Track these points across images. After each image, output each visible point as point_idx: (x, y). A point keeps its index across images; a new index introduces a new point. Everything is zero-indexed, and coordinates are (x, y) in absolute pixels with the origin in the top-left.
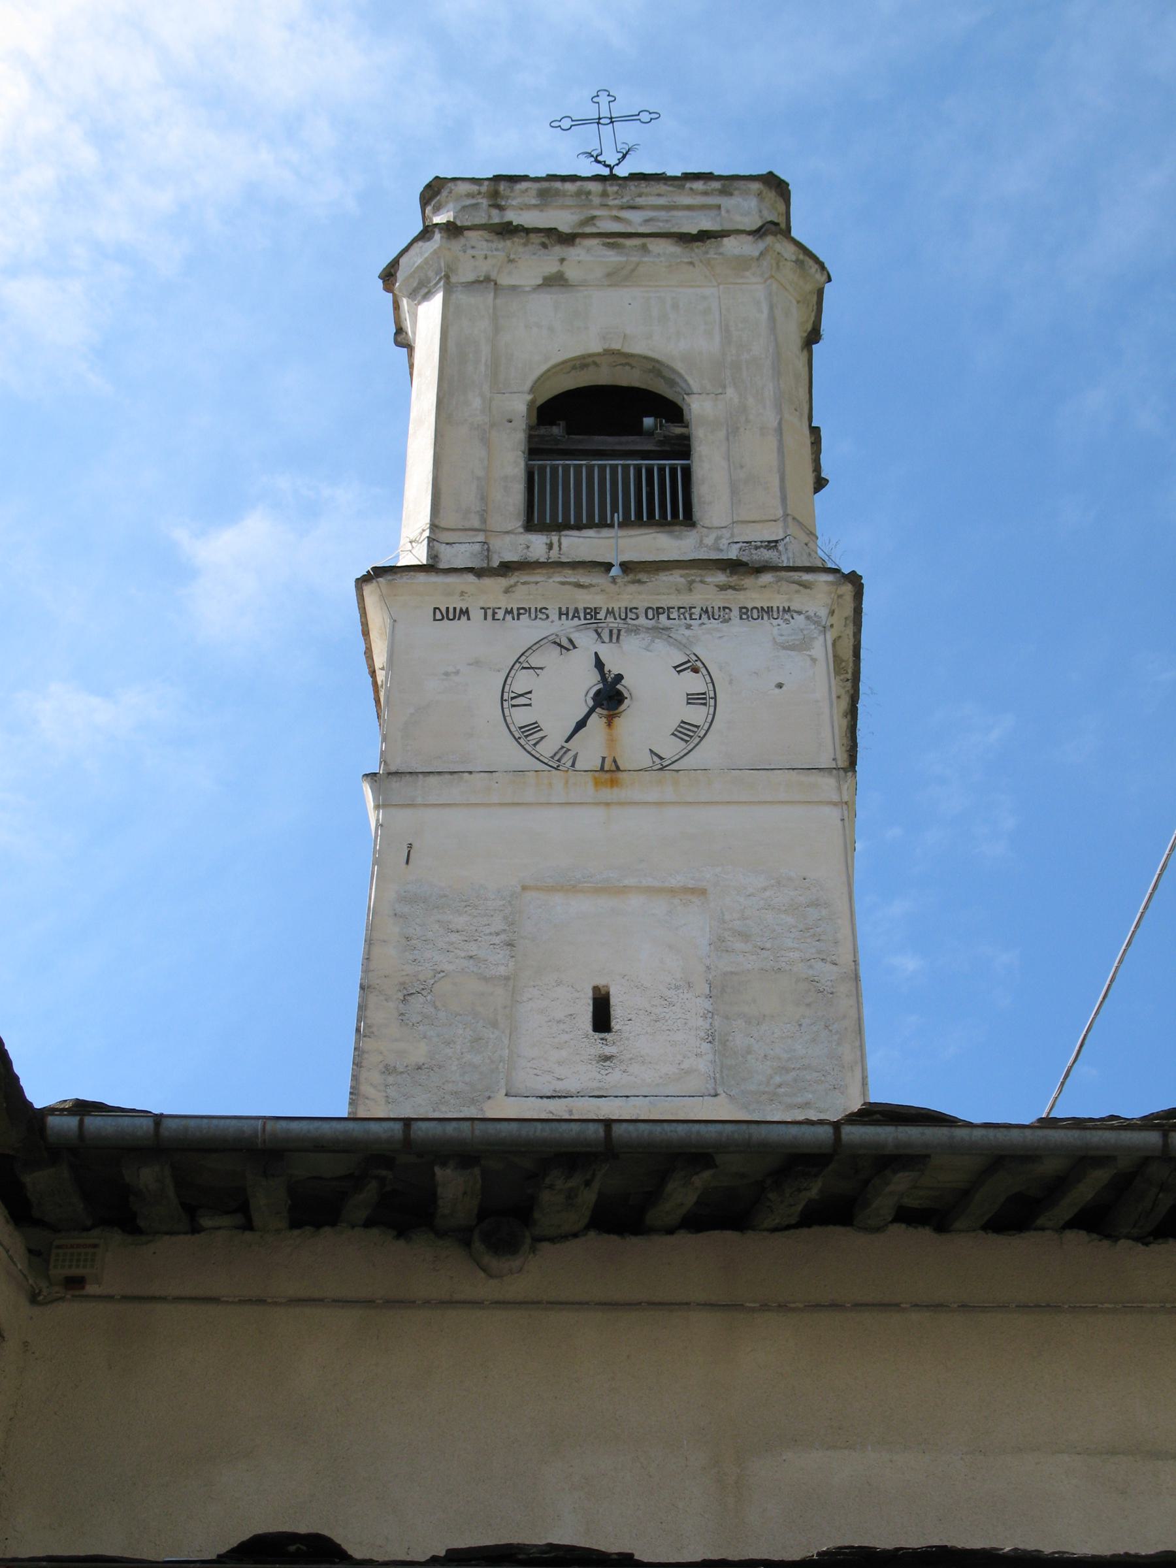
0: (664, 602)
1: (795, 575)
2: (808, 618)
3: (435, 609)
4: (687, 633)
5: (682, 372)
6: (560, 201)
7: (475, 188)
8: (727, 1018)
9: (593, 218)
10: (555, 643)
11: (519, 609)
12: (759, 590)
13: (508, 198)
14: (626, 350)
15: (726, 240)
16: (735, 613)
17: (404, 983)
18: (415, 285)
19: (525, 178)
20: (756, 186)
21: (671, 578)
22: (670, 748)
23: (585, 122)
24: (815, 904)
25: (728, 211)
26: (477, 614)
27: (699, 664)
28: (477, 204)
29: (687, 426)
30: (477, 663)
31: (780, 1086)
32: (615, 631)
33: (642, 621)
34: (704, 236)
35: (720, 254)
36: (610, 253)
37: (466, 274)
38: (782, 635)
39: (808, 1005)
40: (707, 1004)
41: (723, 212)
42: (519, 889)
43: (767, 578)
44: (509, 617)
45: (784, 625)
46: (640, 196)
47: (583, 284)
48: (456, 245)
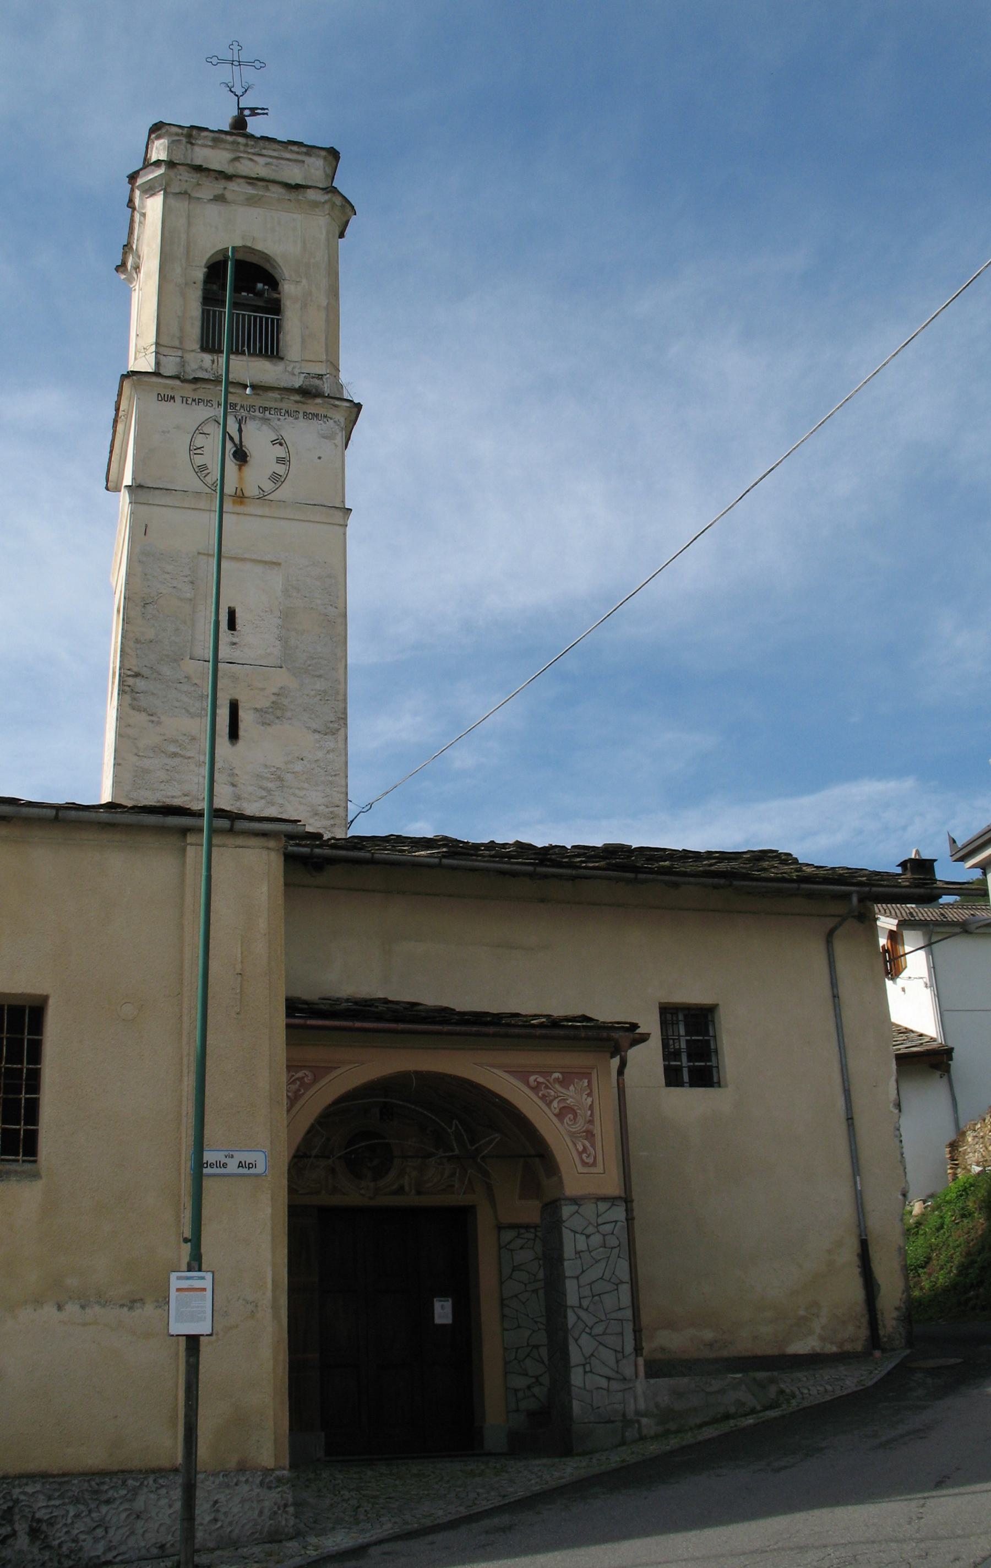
0: (268, 404)
1: (332, 401)
2: (335, 422)
3: (158, 394)
4: (278, 423)
5: (281, 264)
6: (223, 146)
7: (180, 131)
8: (288, 630)
9: (239, 157)
10: (215, 421)
11: (199, 399)
12: (315, 406)
13: (196, 139)
14: (253, 247)
15: (308, 190)
16: (301, 415)
17: (144, 598)
18: (147, 188)
19: (206, 129)
20: (323, 153)
21: (273, 395)
22: (268, 486)
23: (223, 61)
24: (329, 576)
25: (308, 166)
26: (178, 400)
27: (282, 441)
28: (180, 140)
29: (279, 294)
30: (178, 427)
31: (309, 666)
32: (244, 418)
33: (257, 413)
34: (298, 187)
35: (305, 197)
36: (250, 188)
37: (175, 188)
38: (322, 430)
39: (324, 627)
40: (280, 621)
41: (306, 166)
42: (196, 554)
43: (319, 401)
44: (194, 403)
45: (323, 424)
46: (264, 149)
47: (234, 202)
48: (172, 173)
